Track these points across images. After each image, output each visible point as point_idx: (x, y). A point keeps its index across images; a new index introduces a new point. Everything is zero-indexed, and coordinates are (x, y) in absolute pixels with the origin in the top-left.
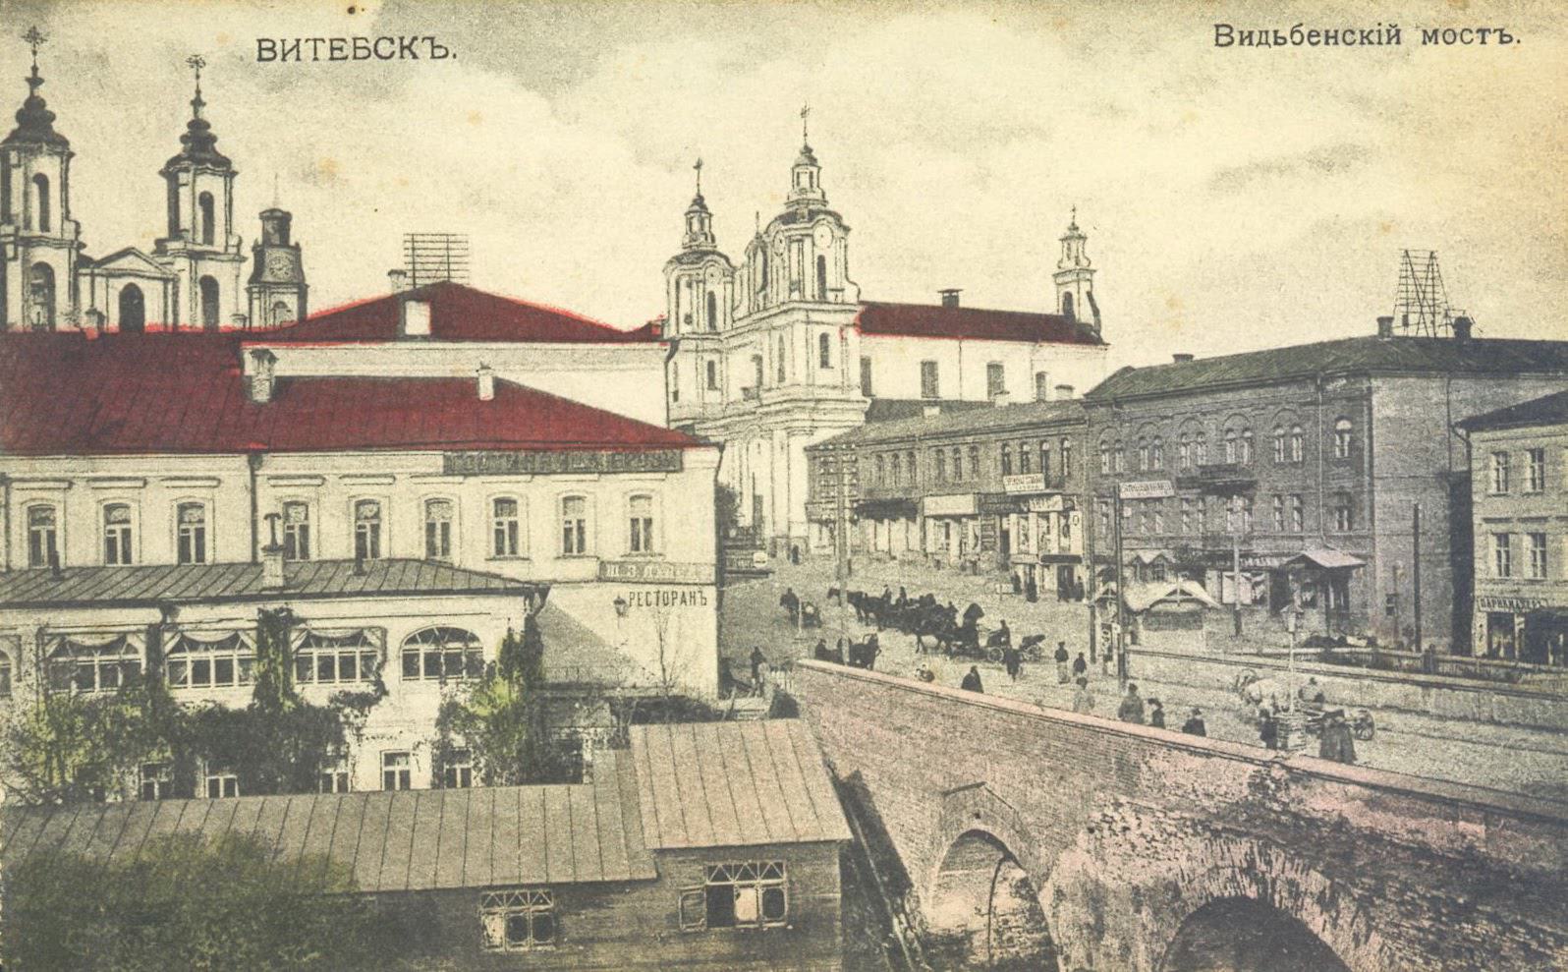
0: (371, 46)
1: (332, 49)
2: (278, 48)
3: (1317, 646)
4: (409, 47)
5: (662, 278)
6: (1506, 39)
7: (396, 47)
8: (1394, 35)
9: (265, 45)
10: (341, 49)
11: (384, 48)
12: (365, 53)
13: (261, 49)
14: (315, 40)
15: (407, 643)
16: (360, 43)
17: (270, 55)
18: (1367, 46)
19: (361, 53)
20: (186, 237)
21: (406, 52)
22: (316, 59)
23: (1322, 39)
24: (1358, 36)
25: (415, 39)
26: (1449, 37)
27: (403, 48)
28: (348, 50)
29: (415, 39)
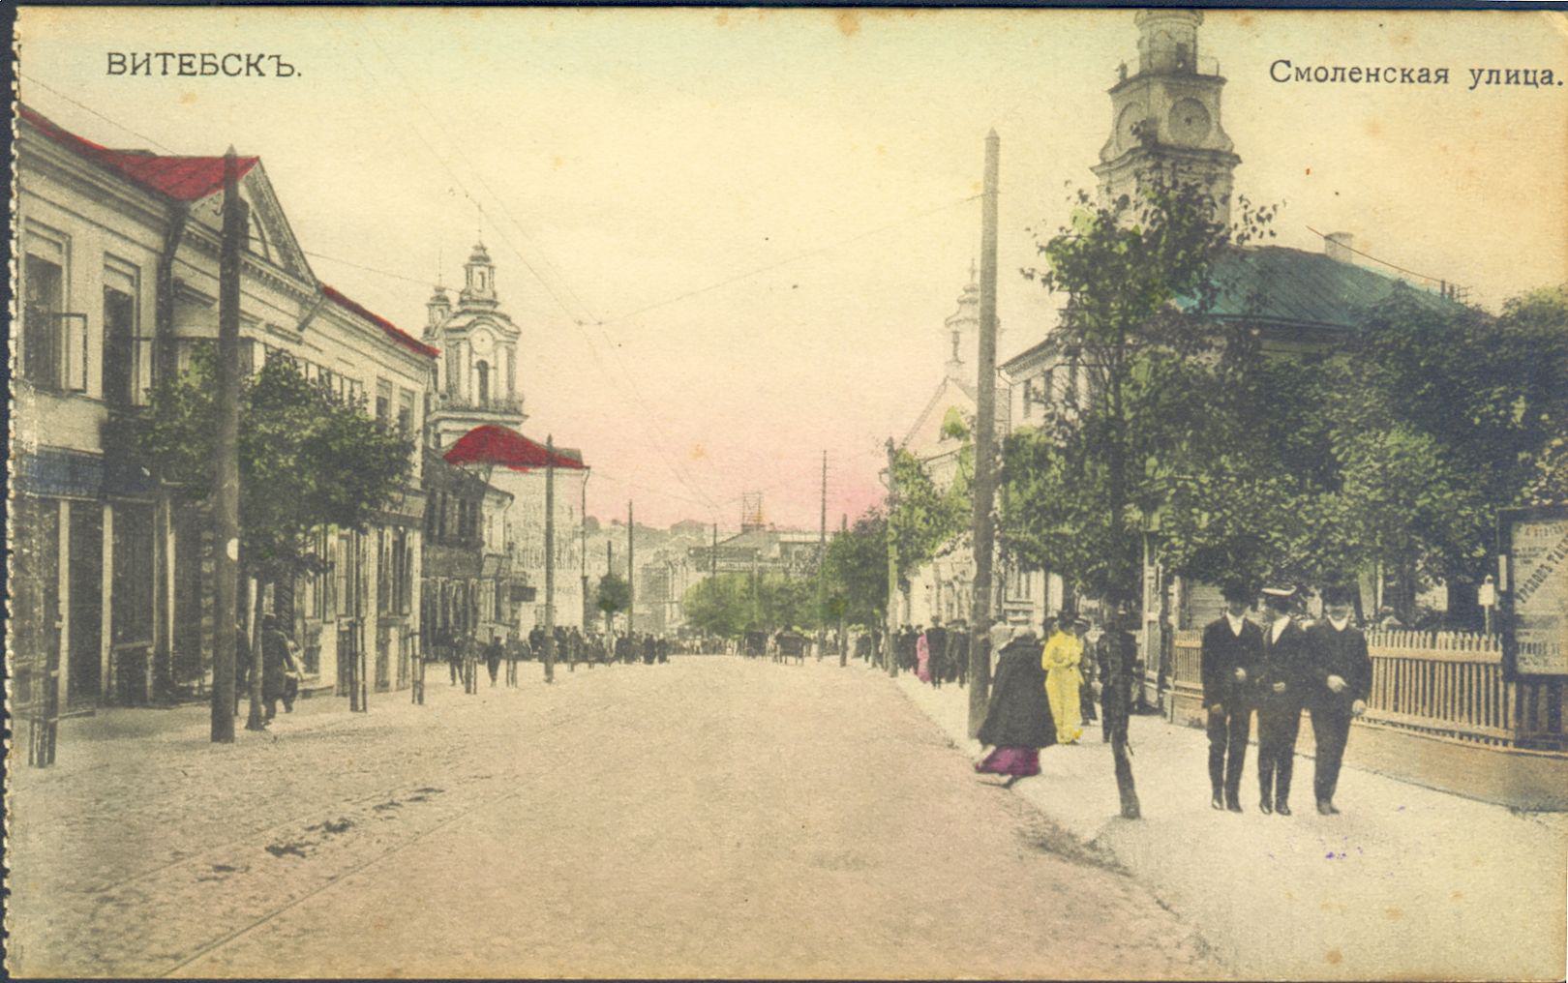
0: (219, 63)
1: (182, 64)
2: (129, 63)
3: (99, 519)
4: (255, 65)
5: (497, 288)
6: (285, 70)
7: (243, 64)
8: (1443, 76)
9: (115, 58)
10: (190, 65)
11: (233, 65)
12: (212, 69)
13: (111, 63)
14: (165, 55)
15: (1269, 807)
16: (208, 59)
17: (120, 68)
18: (1406, 85)
19: (209, 69)
20: (973, 302)
21: (252, 69)
22: (165, 73)
23: (1364, 76)
24: (1399, 75)
25: (261, 56)
26: (1321, 74)
27: (249, 65)
28: (197, 66)
29: (261, 56)
